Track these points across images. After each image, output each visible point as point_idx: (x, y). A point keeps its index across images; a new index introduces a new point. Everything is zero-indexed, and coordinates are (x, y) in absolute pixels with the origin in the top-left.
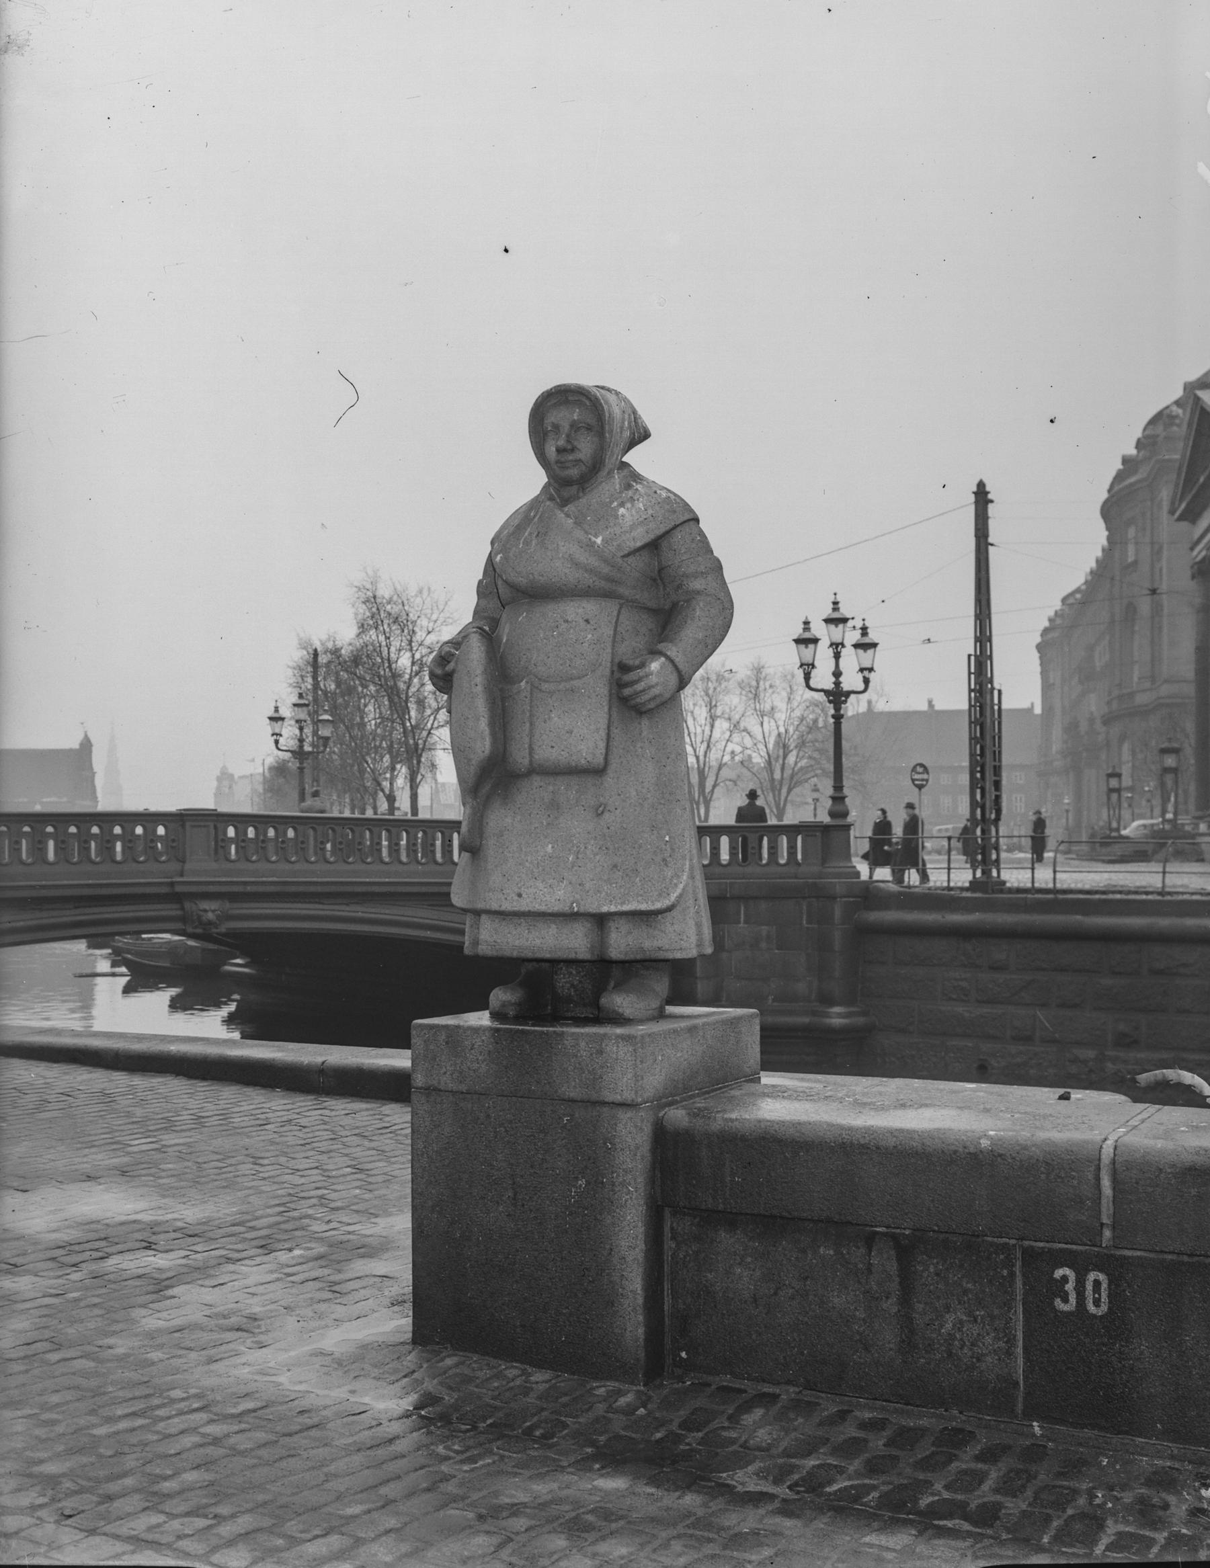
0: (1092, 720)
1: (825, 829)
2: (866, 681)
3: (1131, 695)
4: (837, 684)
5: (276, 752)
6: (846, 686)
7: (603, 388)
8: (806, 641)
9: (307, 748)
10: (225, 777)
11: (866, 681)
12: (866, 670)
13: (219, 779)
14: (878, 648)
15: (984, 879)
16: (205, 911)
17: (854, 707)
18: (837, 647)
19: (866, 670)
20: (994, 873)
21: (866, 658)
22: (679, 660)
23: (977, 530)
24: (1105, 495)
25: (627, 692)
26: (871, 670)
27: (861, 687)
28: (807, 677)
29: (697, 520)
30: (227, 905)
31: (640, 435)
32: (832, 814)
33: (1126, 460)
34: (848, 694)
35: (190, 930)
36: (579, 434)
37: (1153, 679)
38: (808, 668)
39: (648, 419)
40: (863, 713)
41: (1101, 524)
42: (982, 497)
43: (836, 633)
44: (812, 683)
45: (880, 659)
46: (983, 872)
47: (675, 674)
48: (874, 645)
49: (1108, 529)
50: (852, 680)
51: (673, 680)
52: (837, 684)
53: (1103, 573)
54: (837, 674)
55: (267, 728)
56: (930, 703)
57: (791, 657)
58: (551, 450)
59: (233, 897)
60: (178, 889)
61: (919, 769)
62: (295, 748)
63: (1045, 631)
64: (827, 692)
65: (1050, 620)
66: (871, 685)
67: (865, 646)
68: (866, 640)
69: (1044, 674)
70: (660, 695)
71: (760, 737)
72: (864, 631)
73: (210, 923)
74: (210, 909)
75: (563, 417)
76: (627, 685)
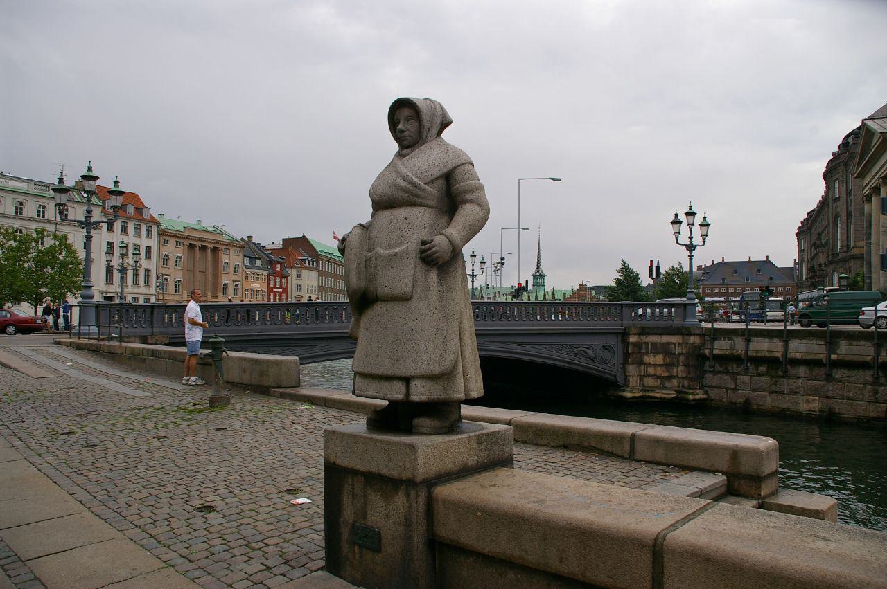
0: (820, 265)
2: (704, 241)
3: (838, 254)
4: (691, 242)
6: (695, 243)
8: (676, 222)
11: (704, 241)
12: (704, 236)
18: (691, 225)
19: (704, 236)
24: (825, 169)
27: (702, 243)
28: (677, 239)
31: (446, 123)
33: (834, 154)
34: (696, 246)
37: (848, 246)
38: (677, 234)
39: (452, 113)
41: (823, 182)
42: (559, 180)
44: (679, 241)
49: (826, 183)
50: (697, 240)
52: (691, 242)
53: (824, 204)
54: (691, 238)
55: (671, 229)
56: (767, 257)
63: (799, 228)
65: (802, 222)
67: (705, 225)
68: (91, 174)
69: (799, 245)
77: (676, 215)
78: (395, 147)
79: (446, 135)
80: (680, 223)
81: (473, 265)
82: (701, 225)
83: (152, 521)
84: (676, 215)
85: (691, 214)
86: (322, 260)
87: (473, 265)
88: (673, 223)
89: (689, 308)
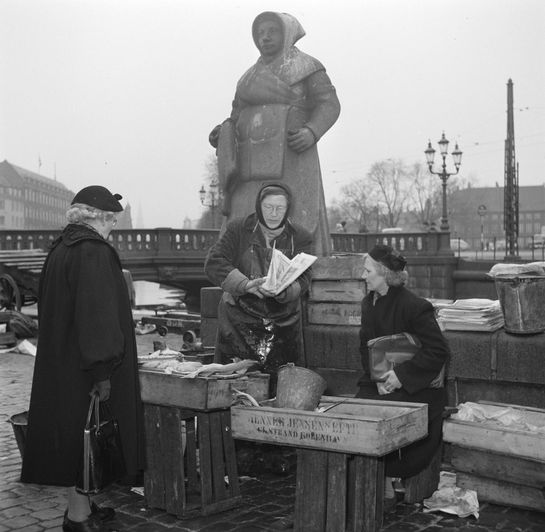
1: (439, 235)
2: (458, 169)
4: (444, 171)
5: (203, 207)
7: (285, 14)
8: (430, 151)
9: (215, 204)
10: (187, 220)
11: (458, 169)
12: (458, 164)
13: (185, 222)
14: (463, 155)
15: (511, 256)
16: (167, 271)
17: (451, 179)
19: (458, 164)
20: (516, 253)
21: (457, 158)
22: (315, 130)
23: (508, 100)
25: (291, 144)
26: (459, 164)
27: (455, 171)
29: (324, 70)
30: (176, 269)
31: (300, 35)
32: (442, 228)
35: (160, 279)
36: (273, 34)
39: (305, 27)
40: (466, 189)
42: (510, 85)
43: (443, 148)
45: (464, 159)
46: (511, 253)
47: (313, 136)
48: (461, 153)
50: (451, 169)
51: (312, 139)
52: (444, 171)
54: (444, 166)
55: (199, 195)
57: (424, 159)
58: (261, 41)
59: (179, 265)
60: (156, 261)
61: (482, 208)
62: (211, 204)
64: (440, 175)
66: (460, 171)
68: (458, 151)
70: (306, 145)
71: (418, 200)
72: (457, 147)
73: (169, 276)
74: (169, 270)
75: (263, 26)
76: (291, 141)
77: (430, 145)
78: (256, 54)
79: (298, 45)
80: (434, 151)
81: (444, 158)
82: (453, 154)
83: (37, 521)
84: (430, 145)
85: (444, 142)
86: (28, 188)
87: (444, 158)
88: (427, 152)
89: (444, 238)
